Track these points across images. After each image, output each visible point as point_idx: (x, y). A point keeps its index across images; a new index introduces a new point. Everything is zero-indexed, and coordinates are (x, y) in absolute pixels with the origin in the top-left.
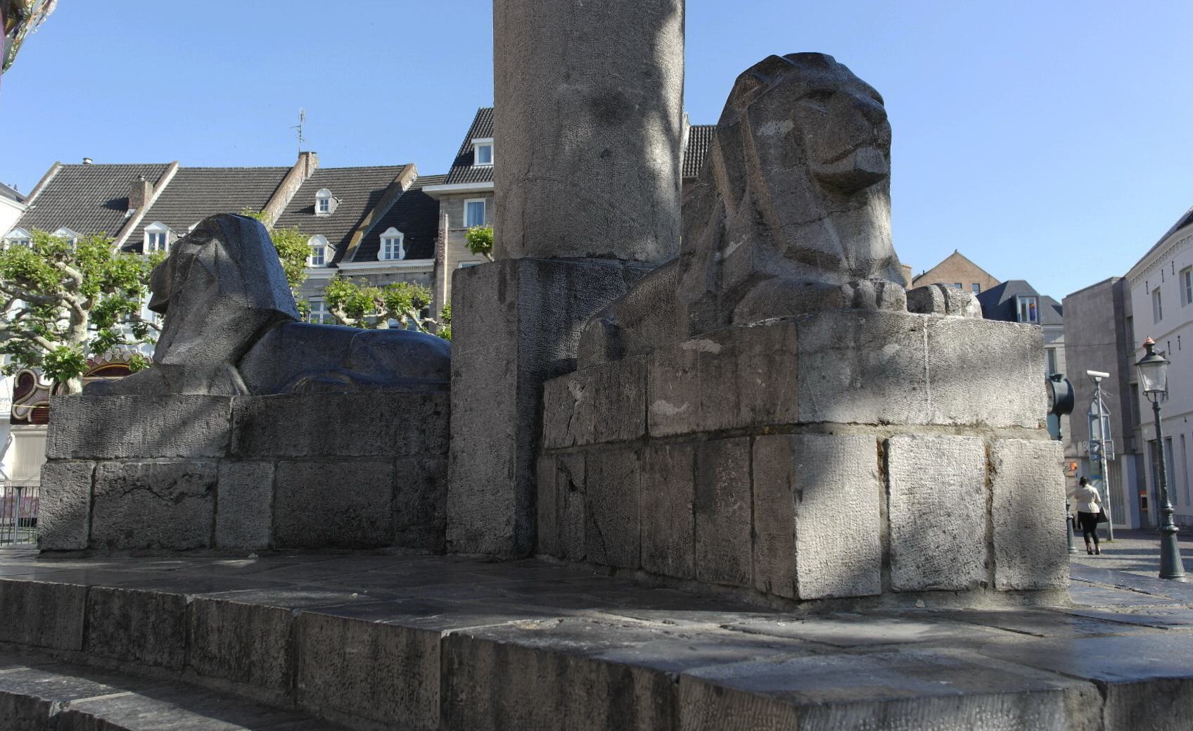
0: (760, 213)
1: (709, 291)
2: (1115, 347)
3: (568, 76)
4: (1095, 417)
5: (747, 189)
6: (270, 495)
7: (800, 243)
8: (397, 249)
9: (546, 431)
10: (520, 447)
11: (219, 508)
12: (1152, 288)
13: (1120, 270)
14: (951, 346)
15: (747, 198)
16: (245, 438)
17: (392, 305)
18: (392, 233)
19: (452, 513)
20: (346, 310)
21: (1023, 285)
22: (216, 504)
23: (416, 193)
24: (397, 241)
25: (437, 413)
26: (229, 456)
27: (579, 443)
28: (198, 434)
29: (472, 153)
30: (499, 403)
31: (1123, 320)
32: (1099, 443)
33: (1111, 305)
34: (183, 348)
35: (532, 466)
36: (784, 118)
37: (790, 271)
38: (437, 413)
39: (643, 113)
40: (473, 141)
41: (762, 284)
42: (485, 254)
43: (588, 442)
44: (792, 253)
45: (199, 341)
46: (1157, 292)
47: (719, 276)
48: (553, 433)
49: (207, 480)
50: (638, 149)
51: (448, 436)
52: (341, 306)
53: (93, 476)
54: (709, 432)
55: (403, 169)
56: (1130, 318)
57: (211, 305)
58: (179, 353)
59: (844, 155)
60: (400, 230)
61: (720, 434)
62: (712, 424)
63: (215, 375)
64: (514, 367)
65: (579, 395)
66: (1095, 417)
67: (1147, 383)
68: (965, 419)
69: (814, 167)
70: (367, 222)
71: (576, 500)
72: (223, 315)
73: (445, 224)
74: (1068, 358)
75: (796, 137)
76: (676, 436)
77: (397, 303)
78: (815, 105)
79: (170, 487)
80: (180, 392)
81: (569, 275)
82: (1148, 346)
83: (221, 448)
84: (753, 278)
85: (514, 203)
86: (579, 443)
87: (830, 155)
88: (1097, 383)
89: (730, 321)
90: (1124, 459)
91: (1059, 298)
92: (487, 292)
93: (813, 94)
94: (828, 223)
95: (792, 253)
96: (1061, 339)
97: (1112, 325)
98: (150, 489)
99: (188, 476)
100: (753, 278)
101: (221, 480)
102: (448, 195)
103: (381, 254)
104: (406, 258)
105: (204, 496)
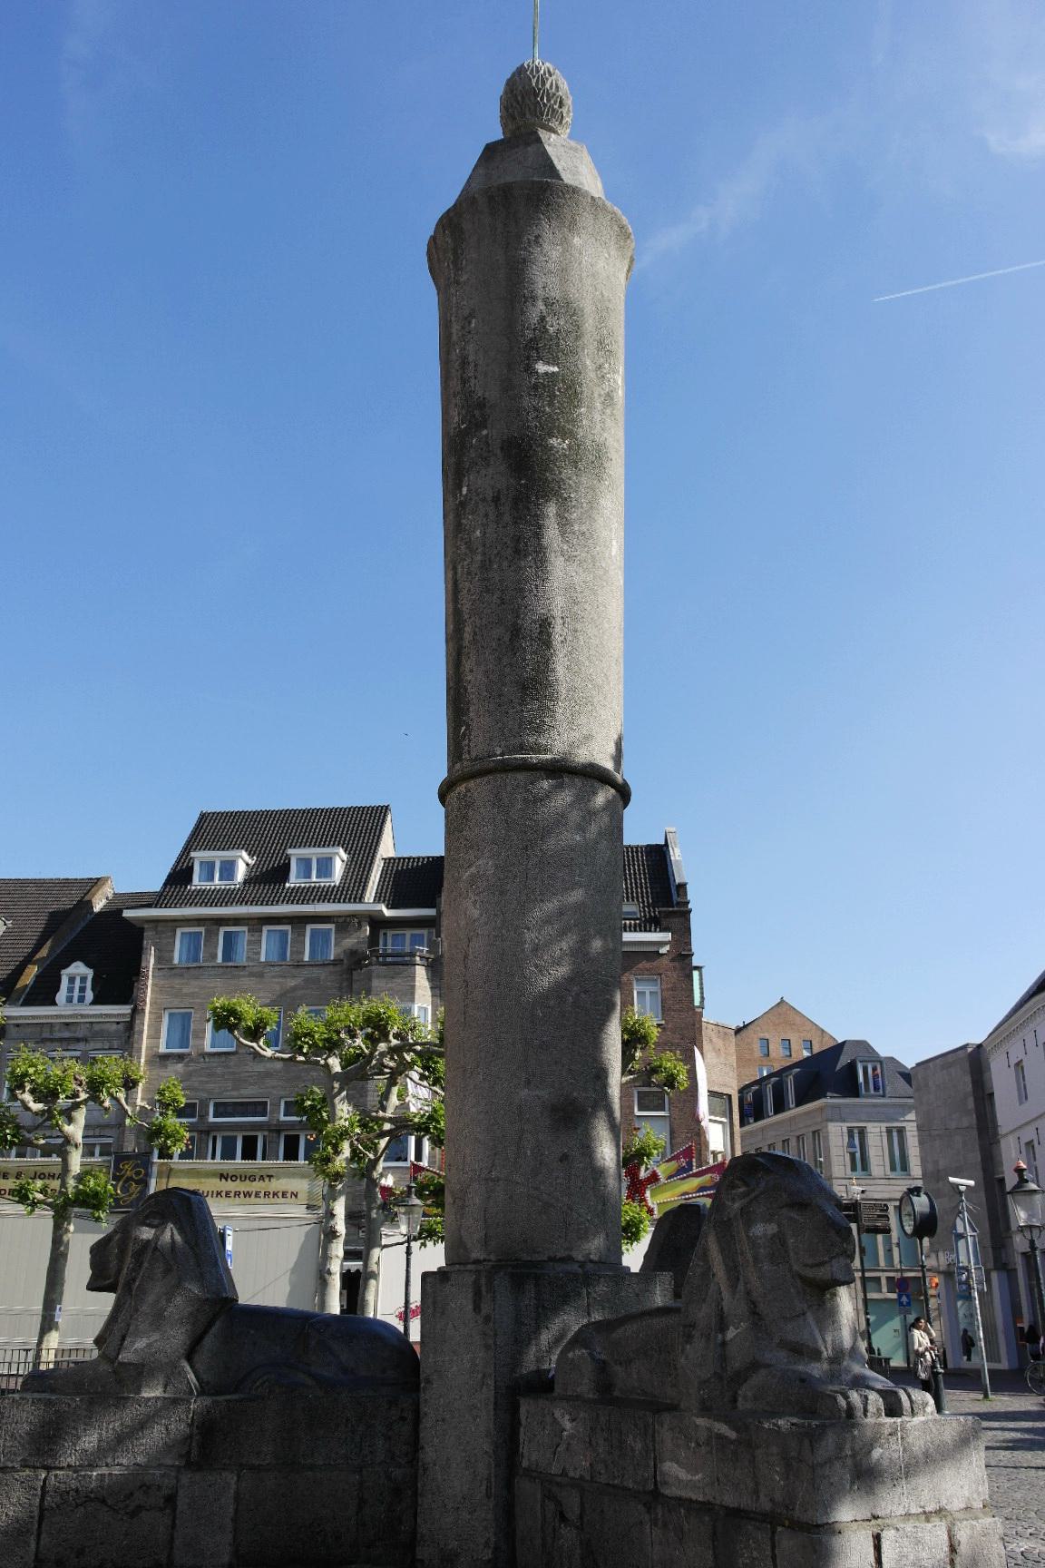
2: (975, 1133)
3: (528, 1082)
4: (961, 1236)
8: (82, 989)
9: (524, 1449)
12: (1013, 1061)
13: (976, 1035)
14: (918, 1442)
15: (741, 1287)
16: (205, 1445)
17: (95, 1086)
18: (79, 969)
19: (423, 1529)
20: (32, 1092)
21: (863, 1045)
23: (113, 914)
24: (83, 979)
25: (403, 1419)
26: (191, 1465)
27: (571, 1474)
28: (155, 1436)
29: (191, 869)
31: (983, 1098)
32: (967, 1269)
33: (968, 1079)
34: (141, 1344)
35: (509, 1485)
36: (770, 1221)
37: (779, 1358)
38: (403, 1419)
39: (593, 1115)
40: (193, 854)
41: (763, 1372)
42: (231, 1031)
44: (783, 1344)
45: (156, 1336)
46: (1019, 1064)
47: (723, 1358)
48: (531, 1454)
49: (165, 1492)
50: (588, 1150)
51: (415, 1445)
52: (28, 1086)
53: (43, 1487)
55: (96, 883)
56: (992, 1095)
57: (170, 1296)
58: (136, 1347)
59: (822, 1264)
60: (88, 965)
61: (736, 1513)
62: (730, 1500)
63: (170, 1373)
64: (491, 1382)
65: (568, 1425)
66: (961, 1236)
67: (1021, 1216)
69: (795, 1267)
70: (44, 952)
71: (568, 1535)
72: (179, 1306)
73: (151, 961)
74: (921, 1143)
75: (779, 1239)
76: (691, 1500)
77: (103, 1083)
78: (794, 1215)
79: (124, 1499)
80: (138, 1391)
81: (536, 1285)
82: (1019, 1171)
84: (755, 1366)
85: (475, 1199)
87: (810, 1261)
88: (961, 1193)
89: (735, 1401)
90: (994, 1275)
91: (909, 1063)
92: (460, 1300)
93: (792, 1205)
94: (810, 1318)
95: (783, 1344)
96: (911, 1116)
97: (971, 1103)
98: (103, 1501)
99: (145, 1488)
100: (755, 1366)
101: (181, 1492)
102: (156, 921)
103: (61, 996)
104: (93, 1003)
105: (161, 1510)
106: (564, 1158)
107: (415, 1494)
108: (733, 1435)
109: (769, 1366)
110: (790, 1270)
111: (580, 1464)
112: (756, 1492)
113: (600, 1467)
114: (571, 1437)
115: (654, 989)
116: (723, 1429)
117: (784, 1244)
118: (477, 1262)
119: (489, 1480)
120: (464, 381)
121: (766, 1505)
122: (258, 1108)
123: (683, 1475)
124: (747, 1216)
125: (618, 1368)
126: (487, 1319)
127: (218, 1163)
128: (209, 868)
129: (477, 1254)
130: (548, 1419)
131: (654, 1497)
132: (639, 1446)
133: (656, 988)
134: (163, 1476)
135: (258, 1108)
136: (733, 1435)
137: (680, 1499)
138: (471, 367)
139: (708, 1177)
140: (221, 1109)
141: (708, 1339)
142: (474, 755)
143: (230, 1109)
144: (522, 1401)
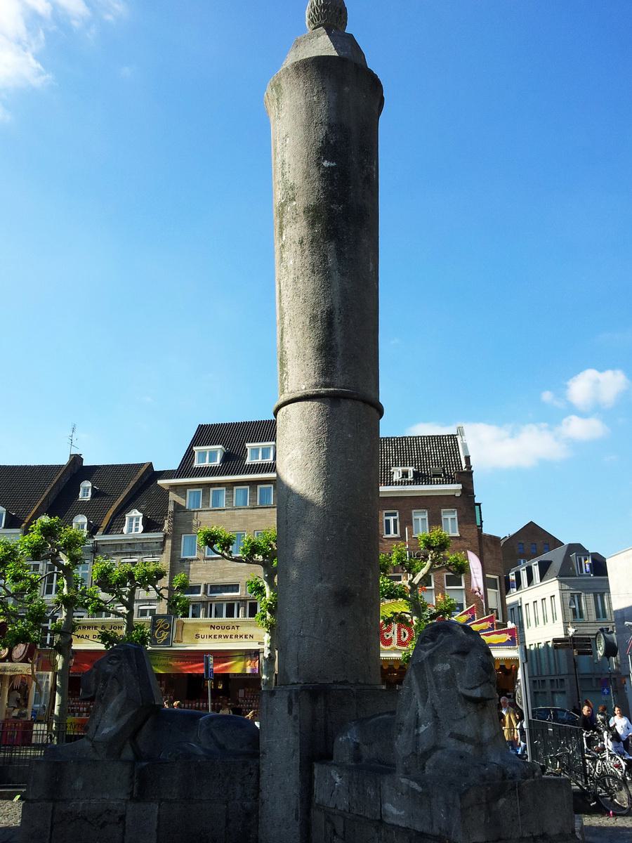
0: (435, 711)
1: (413, 752)
5: (429, 696)
6: (156, 823)
7: (456, 731)
8: (137, 524)
9: (316, 792)
10: (302, 802)
11: (127, 831)
15: (429, 701)
22: (124, 829)
25: (251, 774)
27: (339, 808)
30: (289, 775)
35: (308, 813)
36: (445, 662)
38: (251, 774)
40: (194, 448)
41: (439, 752)
43: (345, 811)
47: (417, 744)
48: (320, 795)
51: (258, 789)
54: (417, 832)
64: (298, 754)
65: (338, 780)
68: (537, 833)
69: (461, 690)
76: (398, 826)
83: (128, 794)
84: (435, 748)
86: (339, 808)
87: (469, 686)
89: (424, 768)
95: (452, 735)
98: (86, 819)
99: (109, 811)
100: (435, 748)
103: (125, 529)
106: (342, 623)
107: (258, 817)
108: (420, 789)
109: (442, 748)
110: (457, 691)
111: (343, 803)
112: (432, 823)
113: (353, 805)
114: (339, 786)
115: (423, 517)
116: (415, 786)
117: (453, 675)
118: (293, 684)
119: (297, 810)
120: (283, 175)
121: (436, 831)
122: (234, 587)
123: (395, 811)
124: (432, 659)
125: (365, 747)
126: (295, 718)
127: (213, 620)
128: (203, 454)
129: (293, 680)
130: (328, 776)
131: (380, 822)
132: (373, 794)
133: (455, 516)
134: (119, 805)
135: (234, 587)
136: (420, 789)
137: (393, 825)
138: (287, 166)
139: (484, 624)
140: (214, 589)
141: (409, 733)
142: (290, 390)
143: (219, 589)
144: (315, 765)
